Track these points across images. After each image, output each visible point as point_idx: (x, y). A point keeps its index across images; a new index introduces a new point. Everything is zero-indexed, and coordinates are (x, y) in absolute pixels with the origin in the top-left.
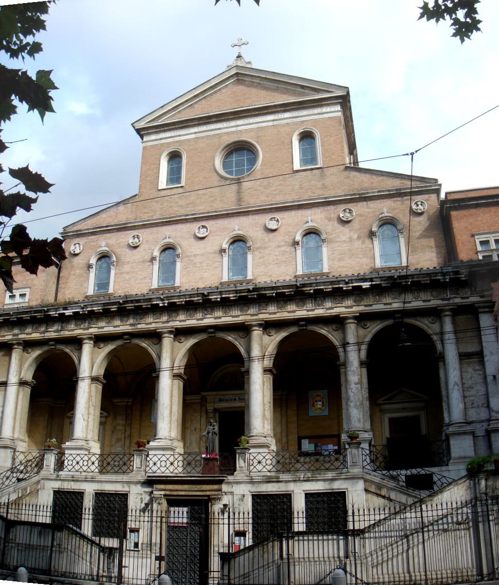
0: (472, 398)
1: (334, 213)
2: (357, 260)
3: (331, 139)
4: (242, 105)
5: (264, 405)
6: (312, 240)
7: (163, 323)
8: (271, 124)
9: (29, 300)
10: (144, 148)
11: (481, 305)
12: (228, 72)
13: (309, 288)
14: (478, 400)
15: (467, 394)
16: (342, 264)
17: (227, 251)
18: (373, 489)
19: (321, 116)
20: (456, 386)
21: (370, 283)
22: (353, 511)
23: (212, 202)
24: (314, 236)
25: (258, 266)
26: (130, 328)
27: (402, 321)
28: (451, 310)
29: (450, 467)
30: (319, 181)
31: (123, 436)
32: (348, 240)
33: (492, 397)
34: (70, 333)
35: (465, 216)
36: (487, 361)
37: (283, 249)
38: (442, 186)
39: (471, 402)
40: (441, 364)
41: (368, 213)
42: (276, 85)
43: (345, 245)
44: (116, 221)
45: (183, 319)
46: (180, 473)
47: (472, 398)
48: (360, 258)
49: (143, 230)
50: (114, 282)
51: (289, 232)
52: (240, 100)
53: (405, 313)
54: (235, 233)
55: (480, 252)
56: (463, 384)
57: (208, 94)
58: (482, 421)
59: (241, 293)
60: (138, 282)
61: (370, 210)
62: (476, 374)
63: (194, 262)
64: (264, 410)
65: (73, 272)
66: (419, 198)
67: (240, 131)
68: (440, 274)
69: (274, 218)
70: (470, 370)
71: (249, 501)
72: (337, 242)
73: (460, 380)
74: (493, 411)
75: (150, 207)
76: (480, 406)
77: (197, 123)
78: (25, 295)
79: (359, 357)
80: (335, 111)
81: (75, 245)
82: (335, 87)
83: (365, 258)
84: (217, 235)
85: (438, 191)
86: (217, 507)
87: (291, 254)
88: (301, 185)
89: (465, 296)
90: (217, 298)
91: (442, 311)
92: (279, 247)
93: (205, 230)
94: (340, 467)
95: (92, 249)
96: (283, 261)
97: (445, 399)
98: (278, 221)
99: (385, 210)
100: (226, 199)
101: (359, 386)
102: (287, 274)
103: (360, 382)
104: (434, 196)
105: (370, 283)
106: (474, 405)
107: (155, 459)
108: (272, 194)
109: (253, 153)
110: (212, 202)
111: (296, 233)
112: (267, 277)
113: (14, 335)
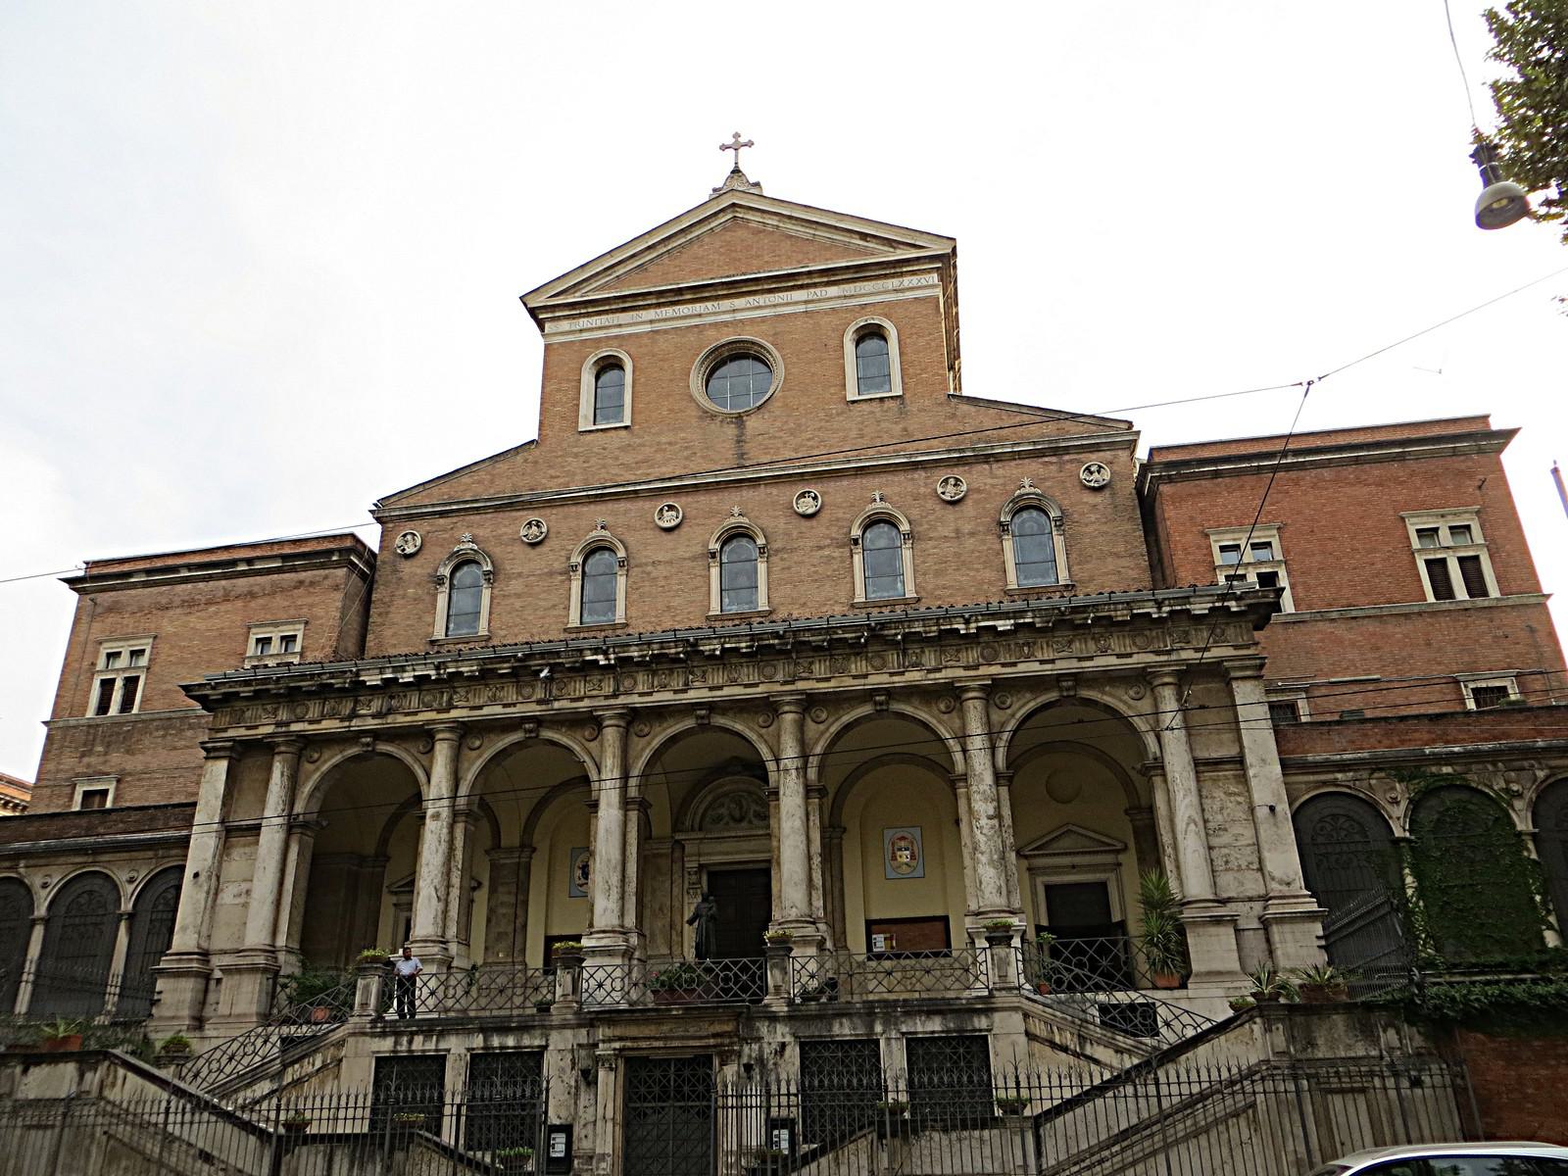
0: (1225, 851)
1: (926, 485)
3: (921, 340)
4: (743, 270)
5: (810, 858)
6: (880, 536)
7: (607, 697)
8: (801, 308)
9: (302, 648)
10: (547, 347)
11: (1237, 663)
12: (715, 202)
13: (893, 632)
15: (1215, 841)
16: (941, 582)
17: (718, 555)
18: (1040, 1029)
19: (901, 296)
20: (1192, 827)
21: (1012, 621)
22: (1017, 1077)
23: (686, 458)
24: (885, 528)
25: (780, 585)
26: (539, 708)
28: (983, 688)
29: (1190, 993)
30: (896, 423)
31: (510, 929)
32: (953, 535)
33: (1269, 850)
34: (409, 719)
35: (1190, 495)
36: (1255, 776)
37: (826, 552)
38: (1142, 434)
40: (1157, 780)
41: (993, 486)
42: (812, 232)
43: (948, 544)
44: (492, 491)
45: (646, 690)
46: (618, 1003)
47: (1225, 851)
48: (978, 570)
49: (548, 511)
50: (490, 613)
52: (740, 260)
53: (1078, 678)
54: (732, 520)
55: (1419, 550)
56: (1206, 821)
57: (675, 244)
58: (1251, 899)
59: (763, 640)
60: (540, 613)
61: (995, 481)
63: (652, 575)
64: (810, 869)
66: (1093, 459)
67: (740, 320)
68: (1151, 604)
69: (809, 492)
70: (1219, 794)
72: (930, 539)
73: (1200, 814)
74: (1273, 879)
75: (563, 467)
77: (654, 301)
78: (143, 651)
79: (994, 765)
80: (929, 283)
81: (404, 536)
82: (930, 237)
83: (988, 570)
84: (698, 525)
85: (1132, 445)
87: (843, 562)
88: (861, 430)
90: (714, 650)
91: (1156, 675)
92: (820, 548)
93: (674, 513)
94: (896, 989)
95: (442, 546)
97: (1169, 851)
98: (815, 498)
99: (1027, 482)
100: (715, 455)
101: (995, 822)
103: (998, 816)
104: (1123, 455)
105: (1012, 621)
106: (1230, 865)
107: (600, 975)
108: (804, 446)
109: (767, 365)
110: (686, 458)
111: (852, 522)
113: (278, 724)
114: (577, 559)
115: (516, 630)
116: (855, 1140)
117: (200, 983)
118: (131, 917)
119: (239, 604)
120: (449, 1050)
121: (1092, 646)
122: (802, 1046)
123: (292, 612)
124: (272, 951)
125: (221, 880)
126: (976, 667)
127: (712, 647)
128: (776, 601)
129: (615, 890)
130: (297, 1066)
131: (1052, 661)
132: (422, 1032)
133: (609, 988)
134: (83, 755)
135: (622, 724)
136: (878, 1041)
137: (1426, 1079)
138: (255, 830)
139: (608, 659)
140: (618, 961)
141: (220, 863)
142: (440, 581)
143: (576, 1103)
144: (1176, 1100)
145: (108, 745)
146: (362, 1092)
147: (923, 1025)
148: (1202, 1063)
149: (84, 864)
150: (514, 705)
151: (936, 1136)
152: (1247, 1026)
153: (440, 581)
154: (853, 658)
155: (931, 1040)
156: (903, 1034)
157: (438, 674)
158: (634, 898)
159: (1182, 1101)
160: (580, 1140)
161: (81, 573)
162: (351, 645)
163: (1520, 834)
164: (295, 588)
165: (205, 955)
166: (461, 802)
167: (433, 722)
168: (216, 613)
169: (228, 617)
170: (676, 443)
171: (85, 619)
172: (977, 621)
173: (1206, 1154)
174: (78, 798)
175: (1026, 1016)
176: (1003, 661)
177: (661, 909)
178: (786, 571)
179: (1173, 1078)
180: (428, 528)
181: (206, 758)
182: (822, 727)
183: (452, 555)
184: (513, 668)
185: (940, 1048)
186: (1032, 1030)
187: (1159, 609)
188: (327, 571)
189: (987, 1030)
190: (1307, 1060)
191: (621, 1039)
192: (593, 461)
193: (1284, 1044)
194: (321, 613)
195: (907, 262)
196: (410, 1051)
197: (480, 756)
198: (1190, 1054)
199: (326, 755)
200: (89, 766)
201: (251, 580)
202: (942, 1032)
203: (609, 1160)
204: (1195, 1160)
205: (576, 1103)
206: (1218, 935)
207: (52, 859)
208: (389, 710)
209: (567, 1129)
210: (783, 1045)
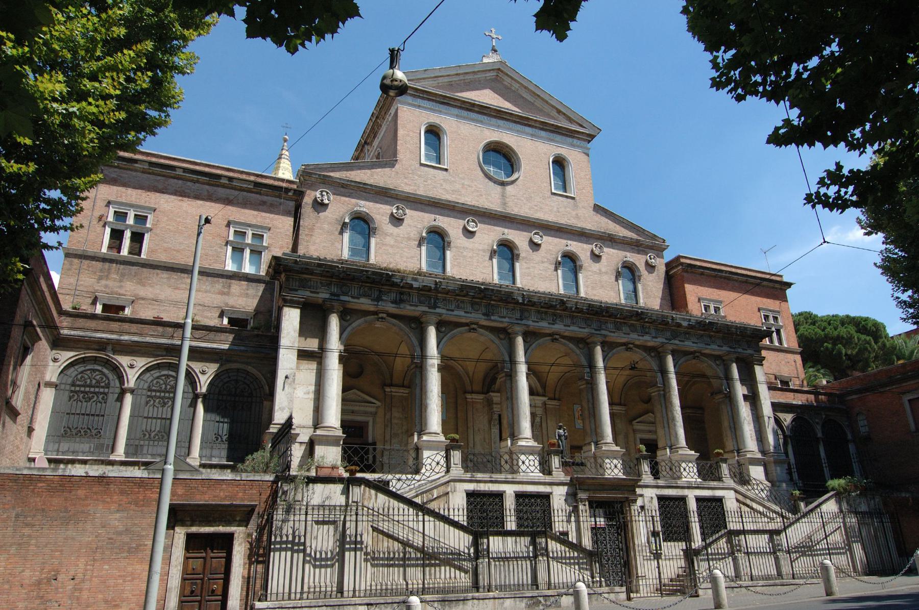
7: (517, 319)
50: (376, 253)
51: (550, 250)
71: (655, 501)
86: (635, 507)
92: (543, 262)
118: (205, 397)
134: (100, 278)
146: (461, 507)
163: (818, 438)
170: (472, 187)
192: (429, 182)
194: (280, 226)
195: (578, 132)
201: (228, 191)
204: (669, 572)
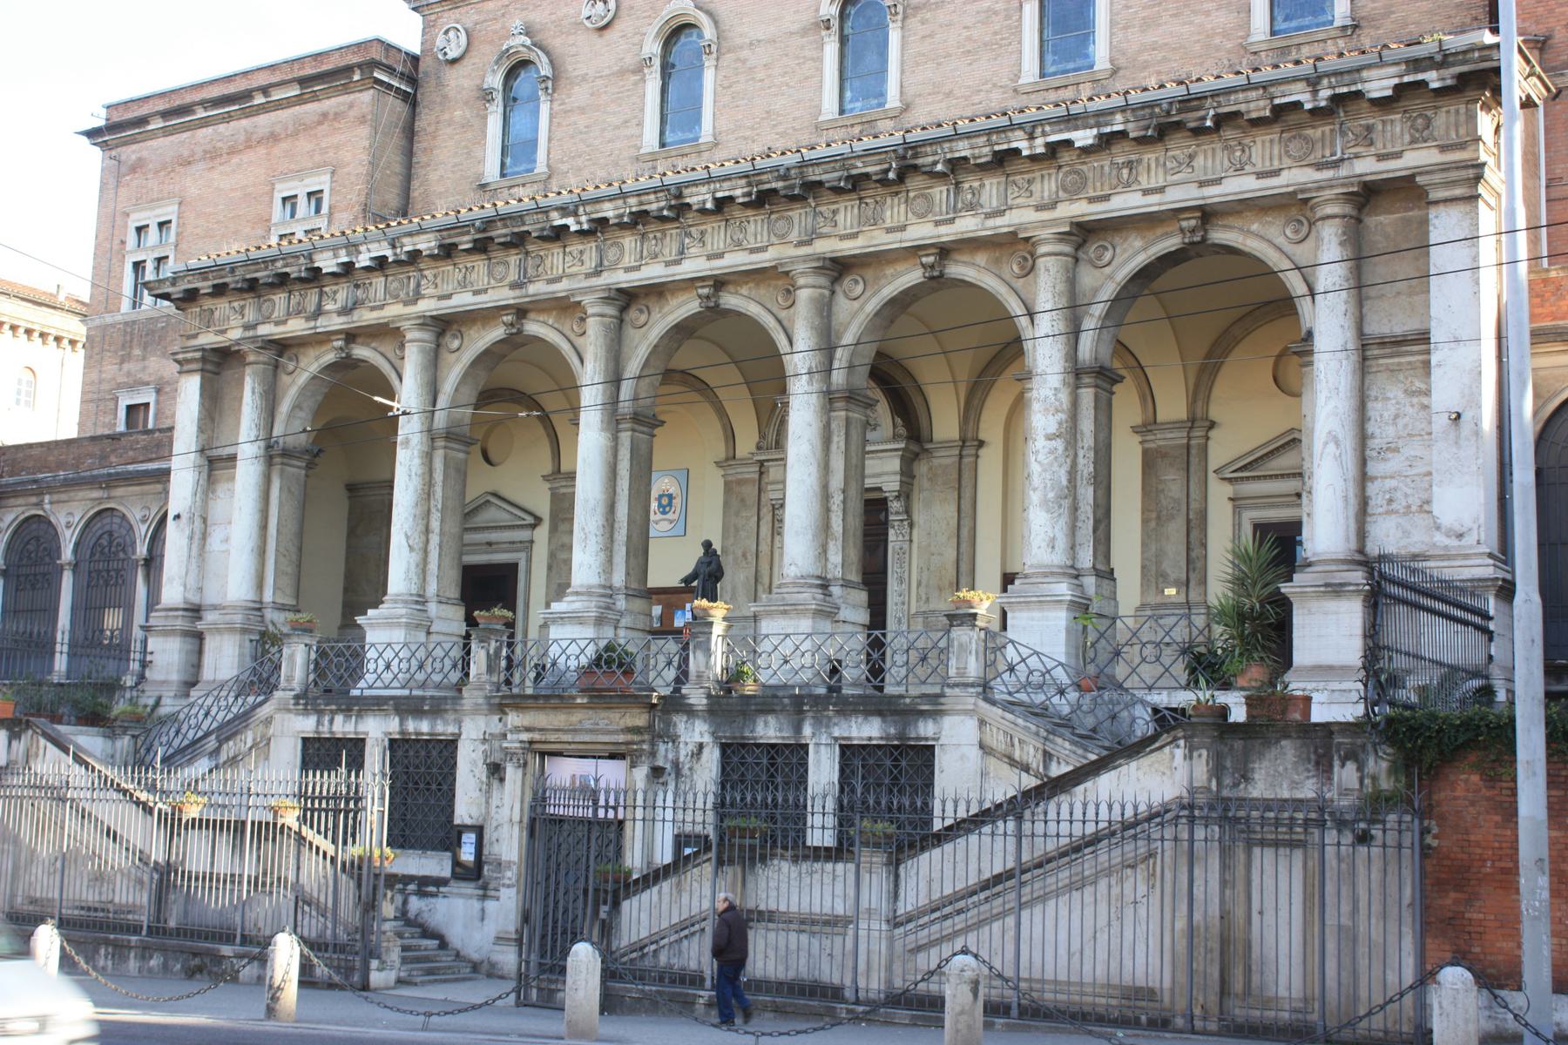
2: (1198, 19)
7: (588, 276)
13: (930, 159)
14: (1409, 491)
16: (1151, 37)
20: (1331, 447)
25: (918, 64)
27: (1204, 239)
34: (375, 314)
39: (1387, 497)
48: (1207, 13)
50: (550, 140)
60: (608, 135)
62: (1412, 406)
65: (446, 116)
76: (1414, 508)
81: (446, 32)
87: (1008, 17)
89: (1390, 149)
90: (704, 202)
96: (986, 45)
102: (995, 85)
105: (1095, 131)
106: (1394, 506)
112: (940, 97)
114: (653, 48)
115: (579, 162)
116: (699, 864)
117: (190, 644)
119: (262, 151)
120: (367, 734)
121: (1222, 159)
122: (724, 748)
123: (317, 158)
124: (258, 607)
125: (209, 523)
126: (1053, 205)
127: (700, 198)
128: (910, 91)
129: (594, 539)
130: (231, 743)
131: (1161, 190)
132: (342, 711)
133: (380, 662)
134: (122, 363)
135: (1067, 249)
136: (807, 745)
137: (1376, 832)
138: (233, 458)
139: (579, 223)
140: (805, 624)
141: (205, 501)
142: (486, 96)
143: (487, 802)
144: (1064, 841)
145: (145, 348)
147: (859, 729)
148: (1103, 797)
149: (100, 500)
150: (485, 291)
151: (785, 866)
152: (1167, 750)
153: (486, 96)
154: (889, 200)
155: (865, 749)
156: (836, 739)
157: (395, 254)
158: (624, 549)
159: (1071, 842)
160: (491, 844)
161: (101, 123)
162: (393, 199)
164: (320, 123)
165: (195, 611)
166: (838, 378)
167: (400, 317)
168: (239, 165)
169: (248, 171)
171: (112, 182)
172: (1044, 134)
173: (1089, 911)
174: (122, 414)
175: (982, 723)
176: (1091, 194)
177: (744, 555)
178: (929, 40)
179: (1065, 814)
180: (476, 17)
181: (179, 373)
182: (856, 304)
183: (500, 58)
184: (475, 241)
185: (879, 759)
186: (989, 741)
187: (1315, 92)
188: (352, 97)
189: (934, 739)
190: (1237, 799)
191: (528, 729)
193: (1205, 777)
196: (331, 732)
197: (458, 360)
198: (1089, 784)
199: (656, 315)
200: (129, 374)
202: (881, 738)
203: (515, 868)
205: (487, 802)
206: (1337, 613)
207: (72, 494)
208: (355, 304)
209: (479, 830)
210: (701, 746)
